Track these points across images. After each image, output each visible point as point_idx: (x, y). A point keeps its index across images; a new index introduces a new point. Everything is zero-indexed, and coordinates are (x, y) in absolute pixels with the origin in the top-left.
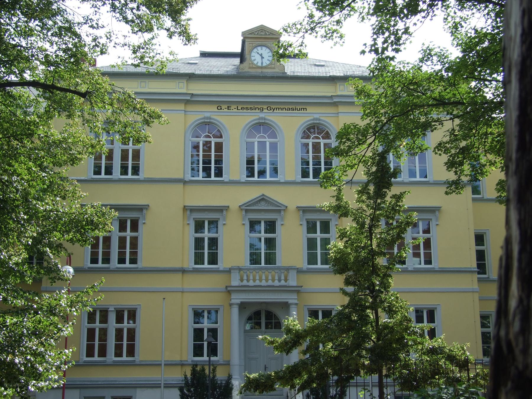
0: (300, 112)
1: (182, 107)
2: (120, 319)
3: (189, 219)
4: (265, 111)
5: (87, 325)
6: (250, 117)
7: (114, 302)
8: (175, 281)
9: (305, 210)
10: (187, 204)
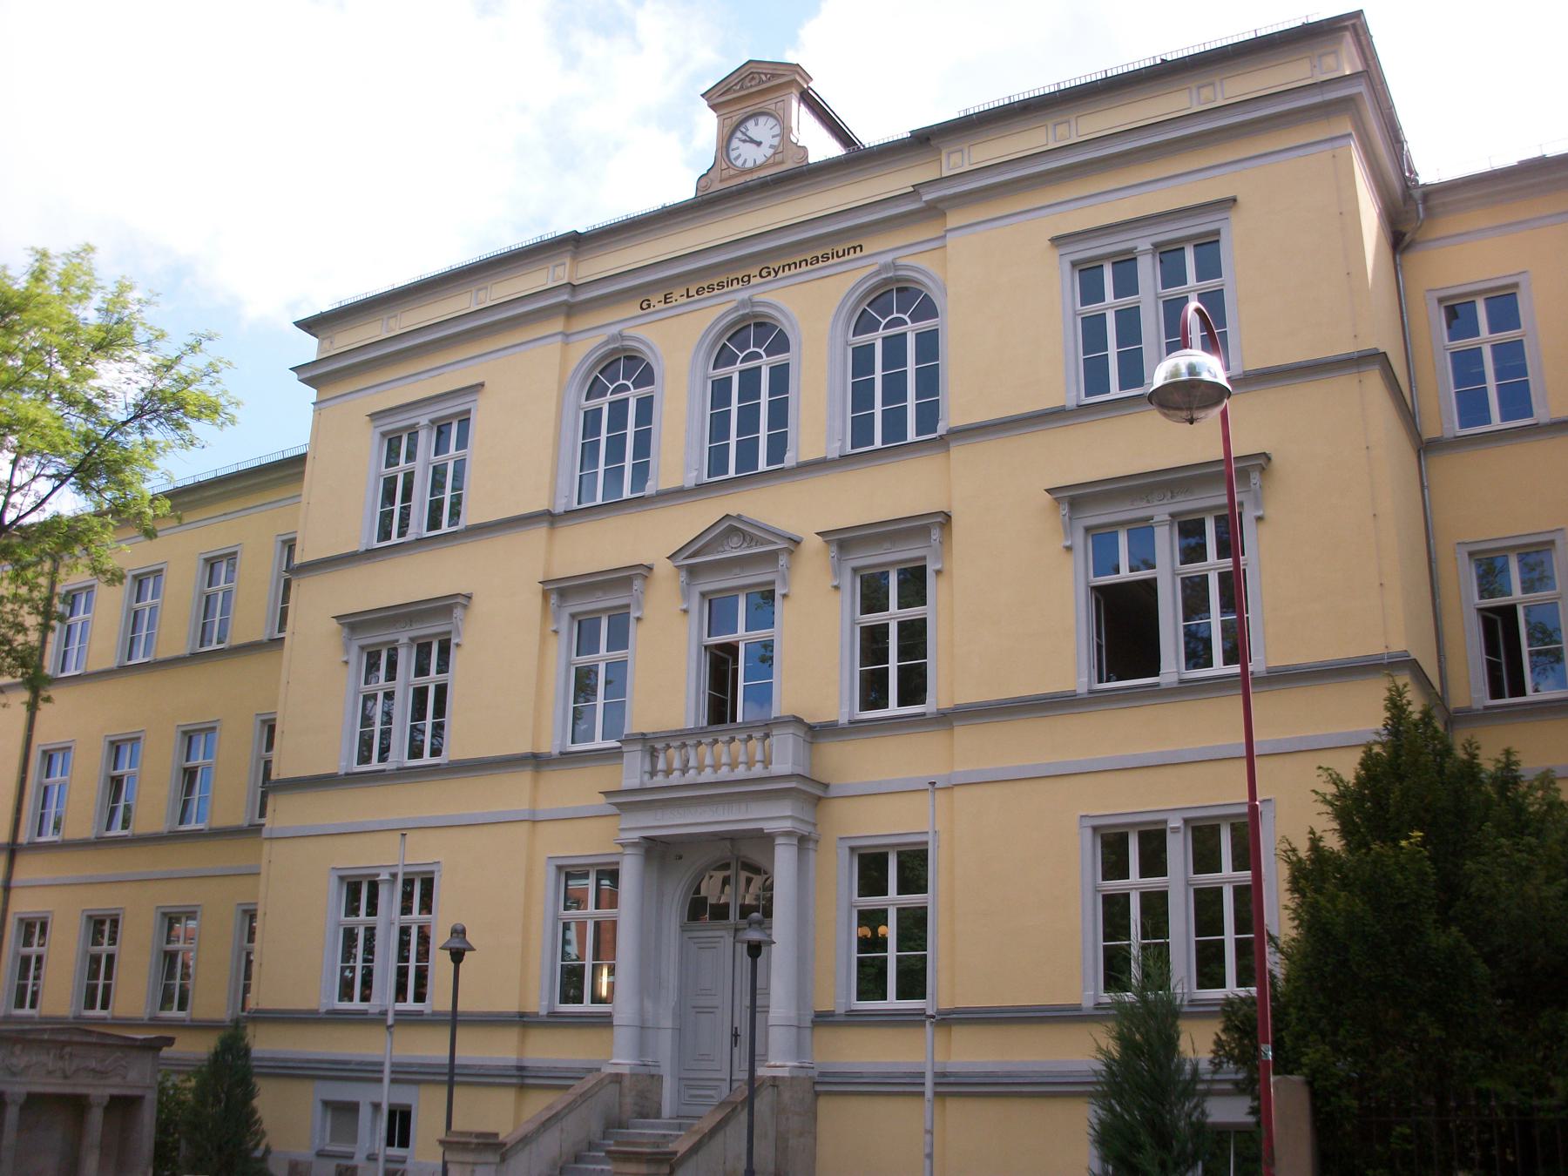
0: (846, 258)
1: (557, 325)
2: (1206, 860)
3: (557, 620)
4: (753, 281)
6: (707, 316)
7: (381, 857)
8: (514, 792)
9: (843, 541)
10: (558, 573)
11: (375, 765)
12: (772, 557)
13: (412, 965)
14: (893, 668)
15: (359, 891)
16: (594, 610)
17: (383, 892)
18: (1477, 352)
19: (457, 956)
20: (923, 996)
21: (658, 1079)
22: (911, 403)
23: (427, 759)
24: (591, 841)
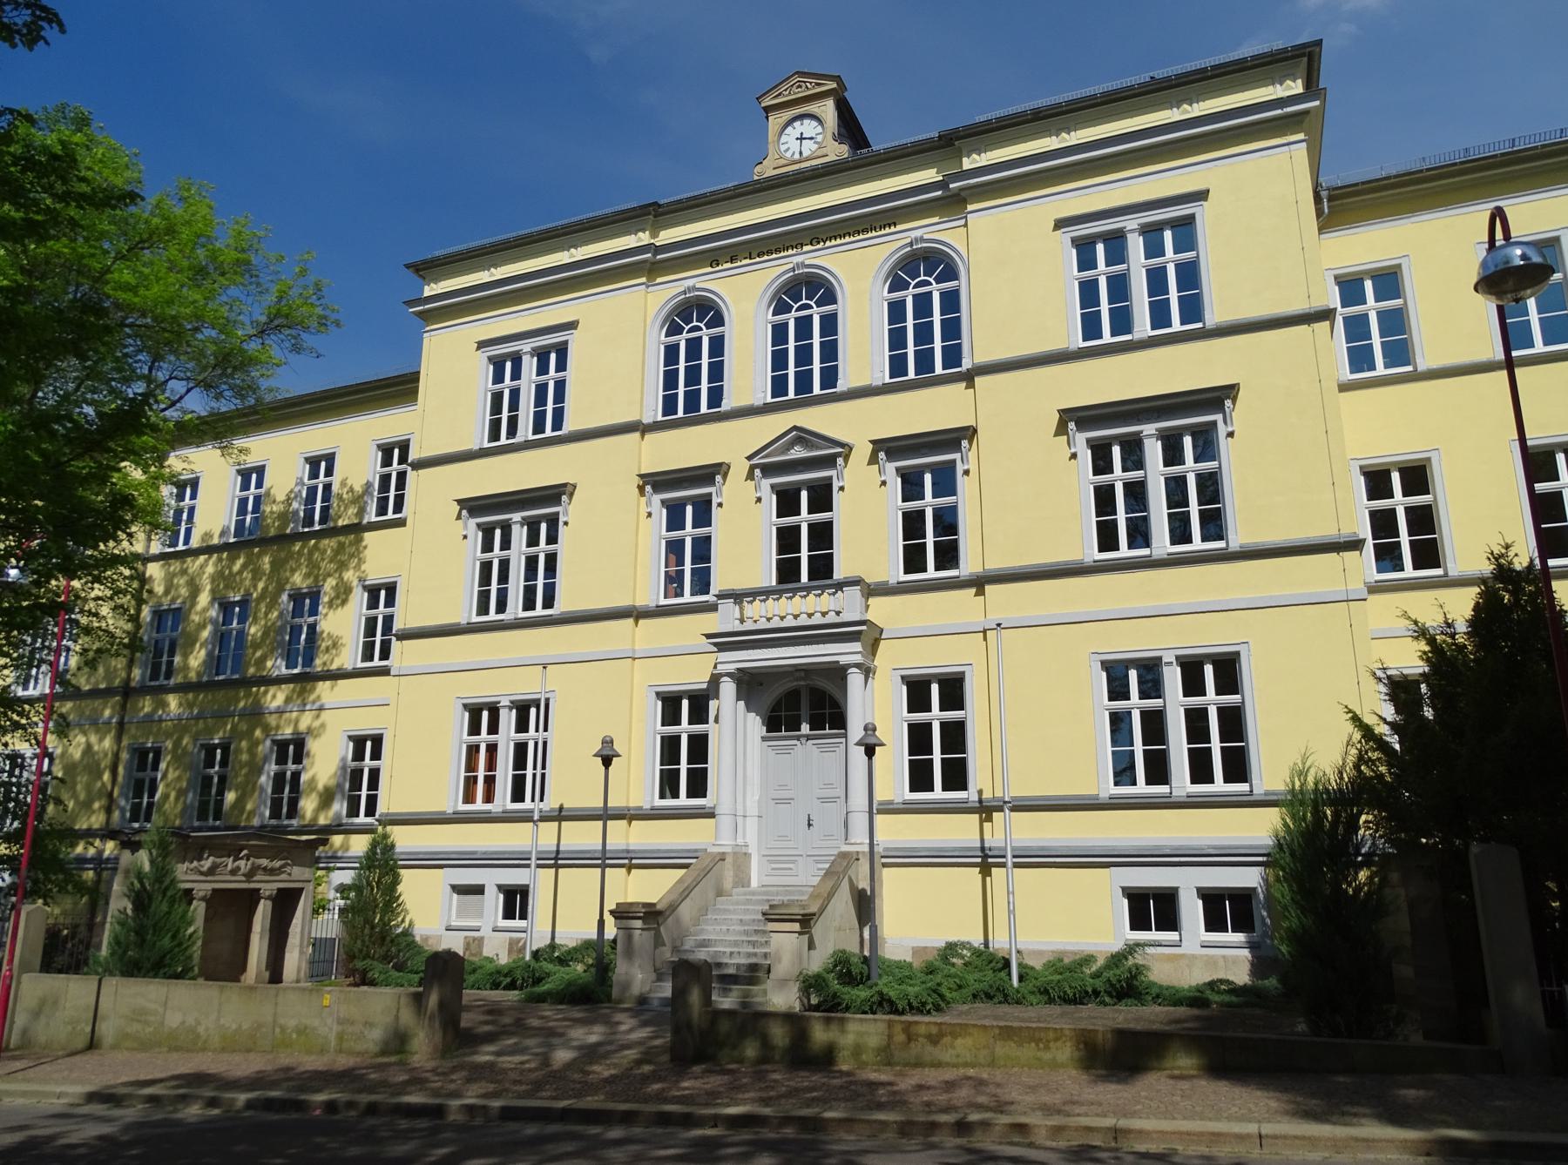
2: (1193, 685)
5: (710, 728)
6: (769, 273)
7: (504, 688)
9: (890, 448)
11: (492, 616)
12: (829, 461)
13: (481, 773)
14: (931, 544)
15: (480, 715)
16: (686, 495)
17: (503, 713)
18: (1365, 317)
19: (870, 751)
20: (965, 788)
21: (747, 855)
22: (816, 366)
23: (539, 611)
24: (693, 675)
